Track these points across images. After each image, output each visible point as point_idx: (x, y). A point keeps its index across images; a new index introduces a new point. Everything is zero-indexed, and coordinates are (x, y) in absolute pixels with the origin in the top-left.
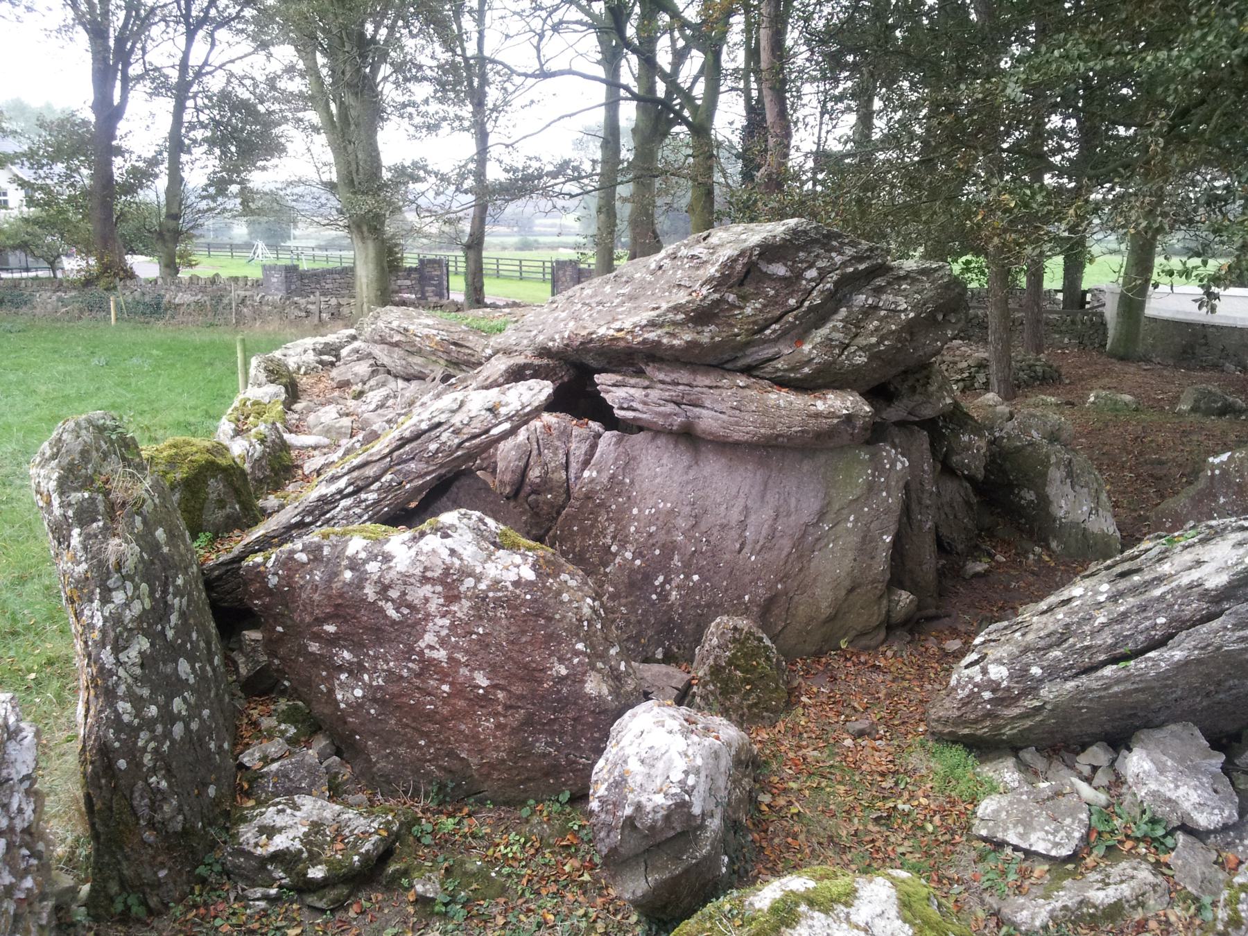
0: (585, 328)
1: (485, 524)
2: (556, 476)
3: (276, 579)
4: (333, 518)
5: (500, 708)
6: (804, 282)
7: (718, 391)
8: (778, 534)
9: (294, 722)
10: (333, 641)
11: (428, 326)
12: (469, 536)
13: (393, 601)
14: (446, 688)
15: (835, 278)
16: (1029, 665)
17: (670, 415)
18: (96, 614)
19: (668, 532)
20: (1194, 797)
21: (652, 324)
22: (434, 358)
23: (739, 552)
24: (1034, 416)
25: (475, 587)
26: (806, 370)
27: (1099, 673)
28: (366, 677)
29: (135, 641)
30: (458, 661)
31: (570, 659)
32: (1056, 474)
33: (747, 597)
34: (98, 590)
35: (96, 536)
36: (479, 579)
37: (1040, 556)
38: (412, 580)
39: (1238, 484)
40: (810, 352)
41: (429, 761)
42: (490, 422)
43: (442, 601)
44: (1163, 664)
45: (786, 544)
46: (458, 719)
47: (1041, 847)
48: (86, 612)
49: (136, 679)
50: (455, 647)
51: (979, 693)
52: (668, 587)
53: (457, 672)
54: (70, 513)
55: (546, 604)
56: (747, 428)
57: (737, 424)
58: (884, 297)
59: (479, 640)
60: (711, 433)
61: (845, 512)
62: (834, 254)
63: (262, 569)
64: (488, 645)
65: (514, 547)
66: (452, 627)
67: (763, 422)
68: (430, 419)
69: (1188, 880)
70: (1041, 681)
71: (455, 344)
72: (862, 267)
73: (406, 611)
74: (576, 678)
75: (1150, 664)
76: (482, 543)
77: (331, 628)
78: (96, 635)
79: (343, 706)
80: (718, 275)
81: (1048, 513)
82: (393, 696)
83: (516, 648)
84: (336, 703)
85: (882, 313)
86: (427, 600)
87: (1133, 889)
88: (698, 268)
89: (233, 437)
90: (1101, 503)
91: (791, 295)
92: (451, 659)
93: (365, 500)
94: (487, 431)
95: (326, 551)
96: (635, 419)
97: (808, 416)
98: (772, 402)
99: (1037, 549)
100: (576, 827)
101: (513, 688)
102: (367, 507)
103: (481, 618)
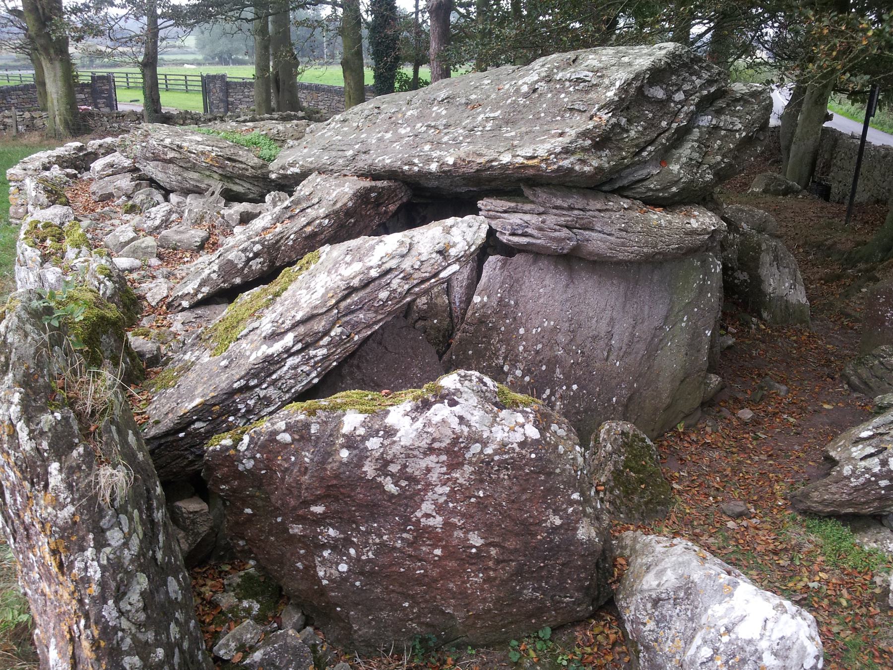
0: (480, 155)
1: (485, 384)
2: (439, 301)
3: (252, 462)
4: (281, 378)
5: (491, 564)
6: (672, 105)
7: (607, 214)
8: (636, 340)
9: (253, 596)
10: (320, 520)
11: (198, 143)
12: (474, 400)
13: (392, 475)
14: (438, 552)
15: (697, 100)
17: (564, 239)
18: (91, 564)
19: (552, 348)
22: (208, 173)
23: (607, 359)
24: (743, 211)
25: (482, 452)
26: (674, 189)
28: (352, 551)
29: (135, 583)
30: (454, 526)
31: (566, 510)
32: (766, 258)
34: (91, 536)
35: (79, 467)
36: (485, 444)
37: (757, 325)
38: (416, 453)
40: (679, 173)
41: (411, 620)
42: (440, 265)
43: (444, 469)
45: (641, 348)
46: (448, 579)
48: (77, 564)
49: (139, 626)
50: (454, 512)
51: (876, 482)
52: (553, 399)
53: (451, 536)
54: (45, 445)
55: (549, 461)
56: (634, 247)
57: (623, 245)
58: (723, 118)
59: (478, 503)
60: (598, 255)
61: (681, 314)
62: (694, 78)
63: (232, 452)
64: (486, 507)
65: (514, 405)
66: (451, 496)
67: (647, 242)
68: (379, 266)
71: (229, 159)
72: (712, 90)
73: (403, 483)
74: (570, 526)
76: (486, 406)
77: (319, 509)
78: (94, 590)
79: (325, 582)
80: (616, 99)
81: (760, 290)
82: (383, 567)
83: (515, 506)
84: (319, 580)
85: (723, 133)
86: (428, 470)
88: (587, 92)
89: (41, 265)
91: (661, 118)
92: (446, 524)
93: (316, 356)
94: (436, 275)
95: (314, 429)
96: (529, 244)
97: (686, 234)
98: (655, 223)
99: (754, 319)
100: (565, 663)
101: (507, 544)
102: (316, 363)
103: (482, 481)
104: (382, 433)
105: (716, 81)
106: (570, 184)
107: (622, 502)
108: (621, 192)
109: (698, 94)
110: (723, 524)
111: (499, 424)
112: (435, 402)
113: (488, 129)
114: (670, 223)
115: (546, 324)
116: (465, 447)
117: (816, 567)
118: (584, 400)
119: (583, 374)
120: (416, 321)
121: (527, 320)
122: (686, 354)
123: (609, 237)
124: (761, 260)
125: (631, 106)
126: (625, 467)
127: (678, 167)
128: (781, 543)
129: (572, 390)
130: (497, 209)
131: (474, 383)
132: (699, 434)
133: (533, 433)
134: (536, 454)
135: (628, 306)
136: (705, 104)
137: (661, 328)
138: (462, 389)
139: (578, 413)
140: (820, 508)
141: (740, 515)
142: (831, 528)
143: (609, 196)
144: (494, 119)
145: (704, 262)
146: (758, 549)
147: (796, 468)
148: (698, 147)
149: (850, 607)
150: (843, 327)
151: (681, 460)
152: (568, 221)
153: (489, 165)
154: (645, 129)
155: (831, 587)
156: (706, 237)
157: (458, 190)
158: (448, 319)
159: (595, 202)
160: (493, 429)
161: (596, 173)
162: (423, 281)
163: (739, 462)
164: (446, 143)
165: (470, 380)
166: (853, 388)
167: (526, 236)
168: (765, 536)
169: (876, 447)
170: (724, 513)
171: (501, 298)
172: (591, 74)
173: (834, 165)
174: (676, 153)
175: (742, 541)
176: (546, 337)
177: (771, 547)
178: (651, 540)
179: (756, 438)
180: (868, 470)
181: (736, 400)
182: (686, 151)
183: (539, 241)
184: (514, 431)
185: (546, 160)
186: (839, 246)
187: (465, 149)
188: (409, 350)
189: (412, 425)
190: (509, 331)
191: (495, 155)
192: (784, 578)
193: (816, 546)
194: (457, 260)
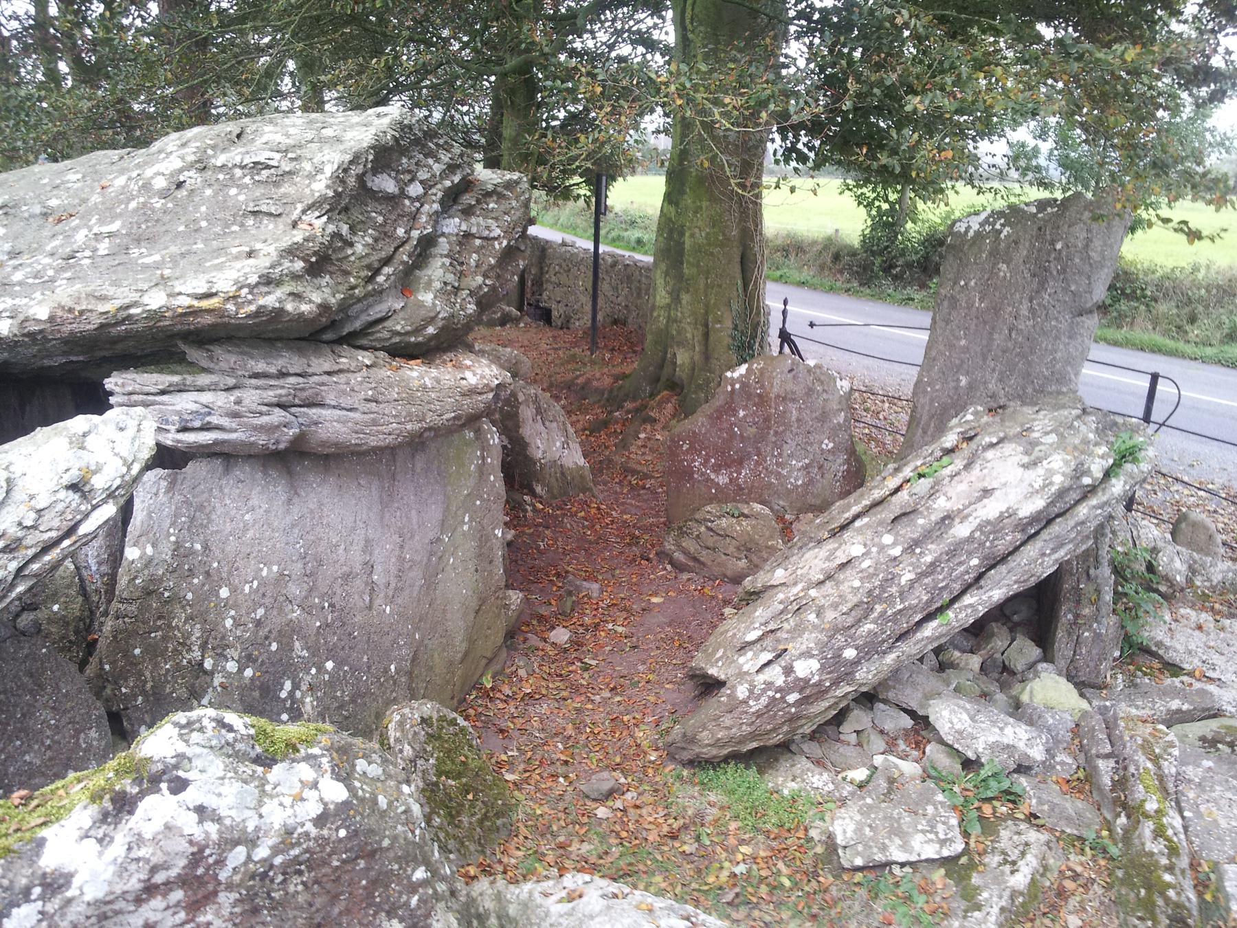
0: (103, 298)
1: (230, 728)
6: (407, 202)
7: (342, 378)
12: (217, 766)
15: (440, 194)
16: (841, 649)
17: (278, 427)
20: (1025, 736)
21: (268, 281)
23: (370, 608)
25: (249, 858)
26: (431, 330)
27: (919, 635)
31: (407, 904)
32: (527, 412)
33: (393, 667)
36: (252, 842)
39: (760, 395)
43: (182, 915)
44: (980, 608)
45: (416, 577)
47: (930, 852)
51: (783, 698)
52: (298, 694)
56: (391, 425)
58: (473, 220)
60: (336, 444)
67: (409, 414)
69: (1063, 823)
70: (856, 663)
72: (457, 179)
75: (969, 611)
76: (242, 768)
81: (526, 457)
87: (1036, 856)
88: (276, 184)
90: (570, 436)
96: (216, 443)
98: (416, 383)
99: (526, 498)
104: (37, 891)
105: (458, 166)
106: (271, 335)
107: (447, 834)
108: (353, 340)
109: (439, 186)
110: (591, 815)
111: (272, 797)
112: (142, 794)
113: (102, 252)
114: (438, 381)
115: (264, 573)
116: (217, 862)
117: (732, 841)
118: (347, 682)
119: (340, 640)
120: (18, 615)
121: (230, 573)
122: (477, 571)
123: (351, 414)
124: (521, 416)
125: (351, 206)
126: (439, 774)
127: (432, 296)
128: (675, 818)
129: (327, 672)
130: (146, 389)
131: (210, 733)
132: (511, 683)
133: (336, 792)
134: (347, 828)
135: (387, 515)
136: (452, 198)
137: (438, 540)
138: (190, 752)
139: (341, 707)
140: (714, 752)
141: (610, 794)
142: (732, 775)
143: (338, 349)
144: (110, 235)
145: (478, 431)
146: (650, 838)
147: (652, 699)
148: (451, 264)
149: (796, 885)
150: (633, 488)
151: (502, 731)
152: (281, 396)
153: (124, 314)
154: (376, 240)
155: (763, 865)
156: (491, 396)
157: (46, 362)
158: (80, 599)
159: (321, 361)
160: (264, 810)
161: (320, 315)
162: (46, 549)
163: (578, 710)
164: (20, 283)
165: (201, 730)
166: (679, 568)
167: (208, 429)
168: (650, 815)
169: (774, 650)
170: (587, 797)
171: (177, 542)
172: (277, 156)
173: (548, 281)
174: (424, 274)
175: (624, 834)
176: (269, 594)
177: (665, 829)
178: (530, 893)
179: (586, 668)
180: (769, 685)
181: (541, 618)
182: (437, 271)
183: (233, 436)
184: (302, 800)
185: (234, 297)
186: (595, 383)
187: (65, 293)
188: (25, 679)
189: (101, 854)
190: (201, 598)
191: (135, 297)
192: (699, 871)
193: (722, 808)
194: (109, 496)
